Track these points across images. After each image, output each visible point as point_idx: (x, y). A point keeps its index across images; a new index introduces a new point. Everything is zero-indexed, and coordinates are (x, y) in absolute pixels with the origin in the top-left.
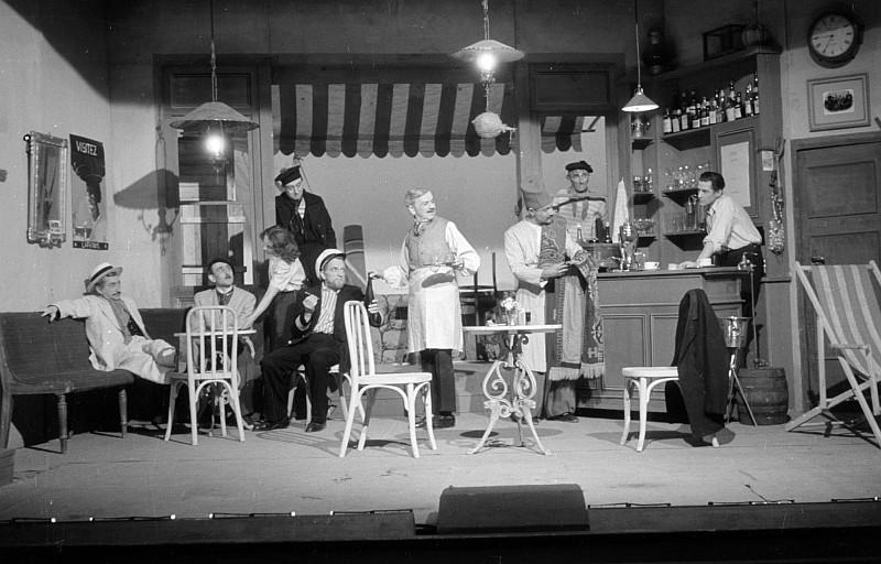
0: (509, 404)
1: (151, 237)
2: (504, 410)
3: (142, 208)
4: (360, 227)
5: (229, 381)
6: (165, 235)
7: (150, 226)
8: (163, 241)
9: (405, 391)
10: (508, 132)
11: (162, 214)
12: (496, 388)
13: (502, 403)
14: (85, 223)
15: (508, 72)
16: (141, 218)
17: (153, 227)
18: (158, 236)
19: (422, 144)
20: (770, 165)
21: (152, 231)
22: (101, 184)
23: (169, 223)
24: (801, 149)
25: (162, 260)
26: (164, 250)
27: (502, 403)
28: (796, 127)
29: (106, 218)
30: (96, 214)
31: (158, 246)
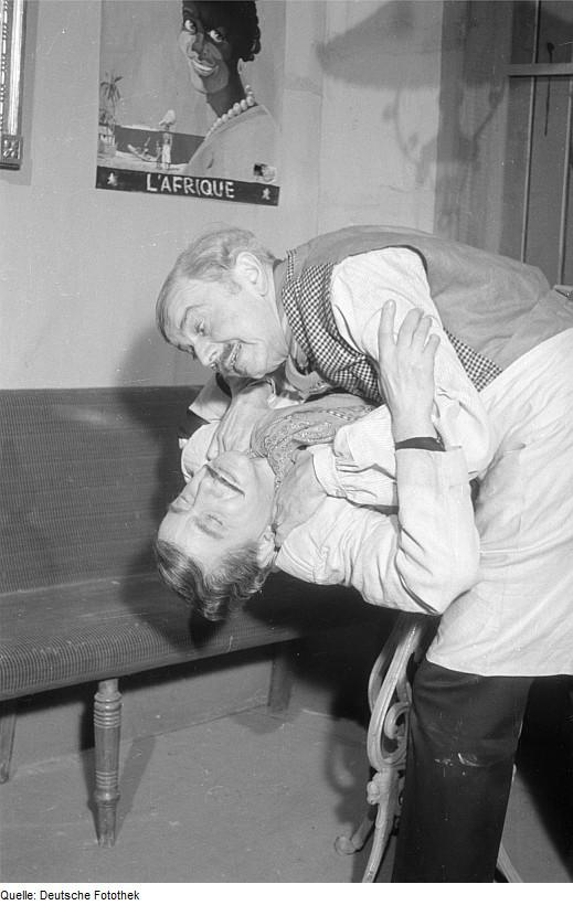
7: (414, 139)
14: (170, 116)
21: (416, 153)
30: (228, 93)
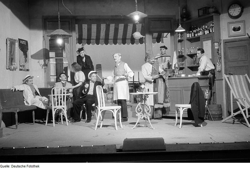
0: (143, 115)
1: (41, 67)
2: (141, 117)
3: (39, 59)
4: (101, 65)
5: (64, 108)
6: (46, 67)
7: (41, 64)
8: (45, 69)
9: (56, 109)
10: (143, 37)
11: (45, 61)
12: (139, 110)
13: (141, 115)
15: (143, 20)
16: (39, 62)
17: (42, 65)
18: (44, 67)
19: (118, 41)
20: (217, 47)
21: (42, 66)
22: (27, 53)
23: (47, 64)
24: (226, 42)
25: (44, 74)
26: (45, 71)
27: (141, 115)
28: (224, 36)
29: (29, 62)
31: (43, 70)
